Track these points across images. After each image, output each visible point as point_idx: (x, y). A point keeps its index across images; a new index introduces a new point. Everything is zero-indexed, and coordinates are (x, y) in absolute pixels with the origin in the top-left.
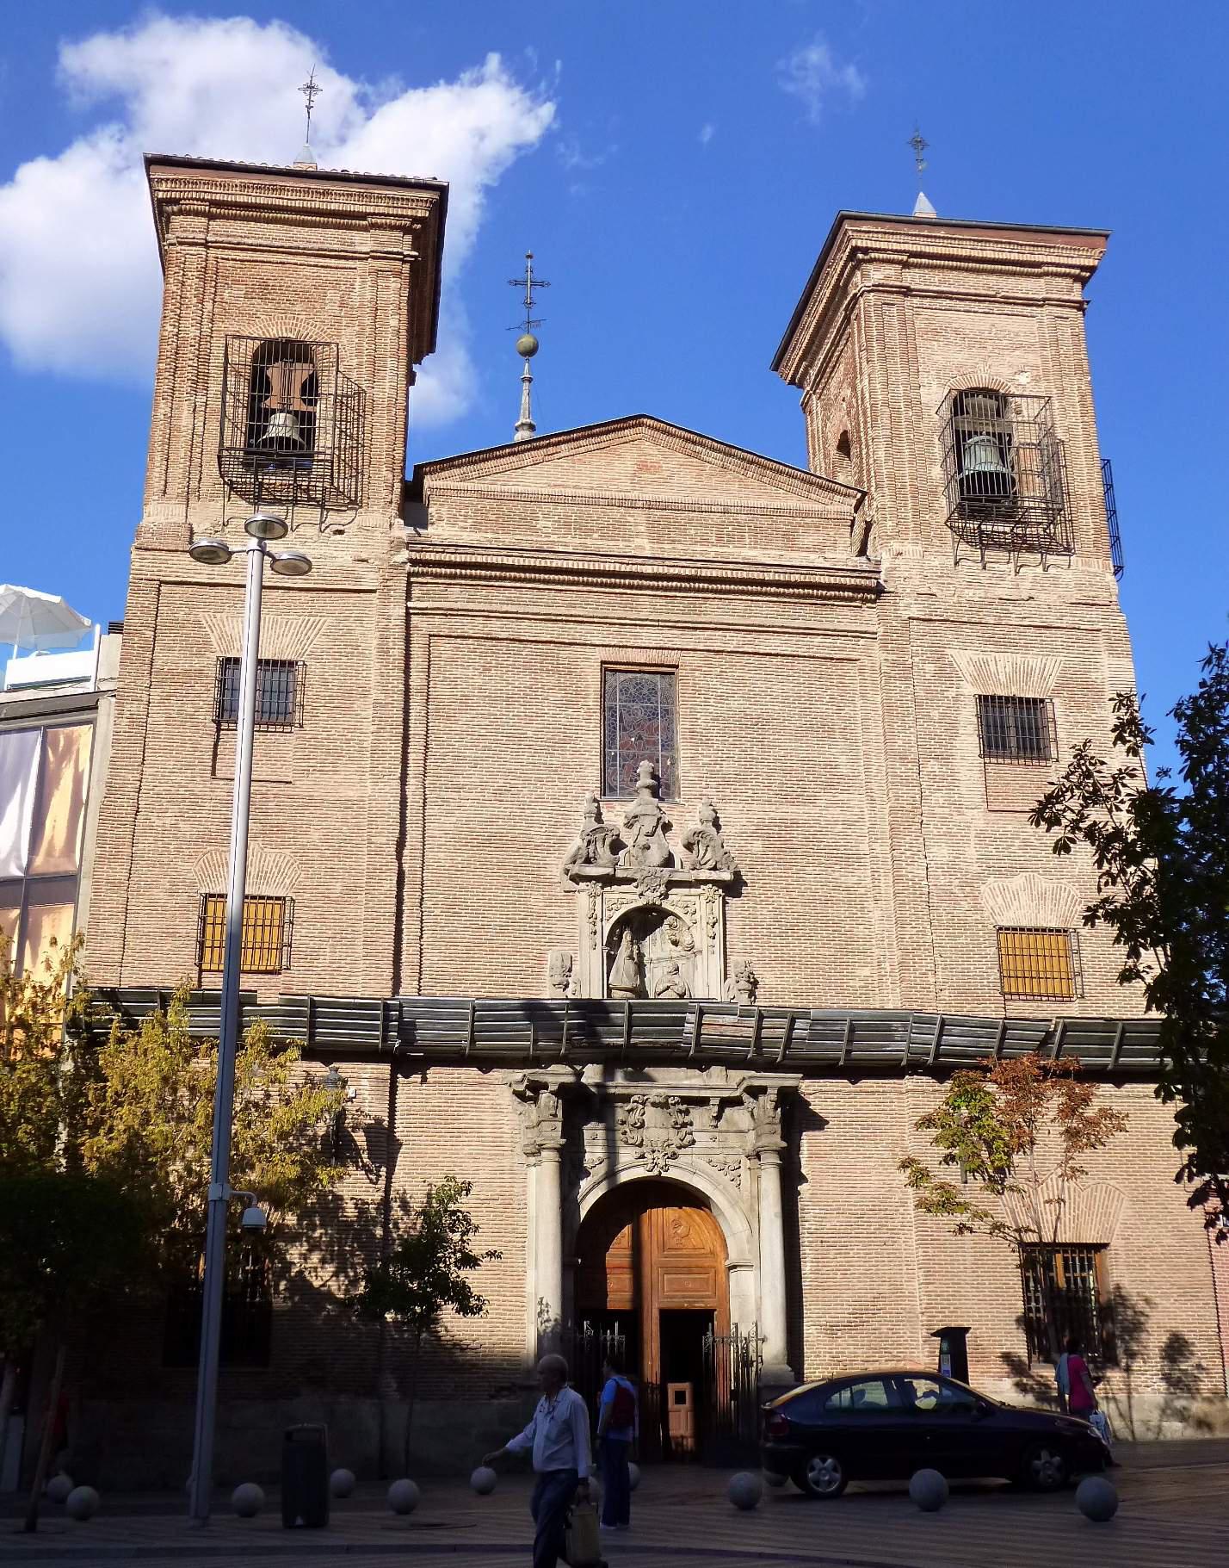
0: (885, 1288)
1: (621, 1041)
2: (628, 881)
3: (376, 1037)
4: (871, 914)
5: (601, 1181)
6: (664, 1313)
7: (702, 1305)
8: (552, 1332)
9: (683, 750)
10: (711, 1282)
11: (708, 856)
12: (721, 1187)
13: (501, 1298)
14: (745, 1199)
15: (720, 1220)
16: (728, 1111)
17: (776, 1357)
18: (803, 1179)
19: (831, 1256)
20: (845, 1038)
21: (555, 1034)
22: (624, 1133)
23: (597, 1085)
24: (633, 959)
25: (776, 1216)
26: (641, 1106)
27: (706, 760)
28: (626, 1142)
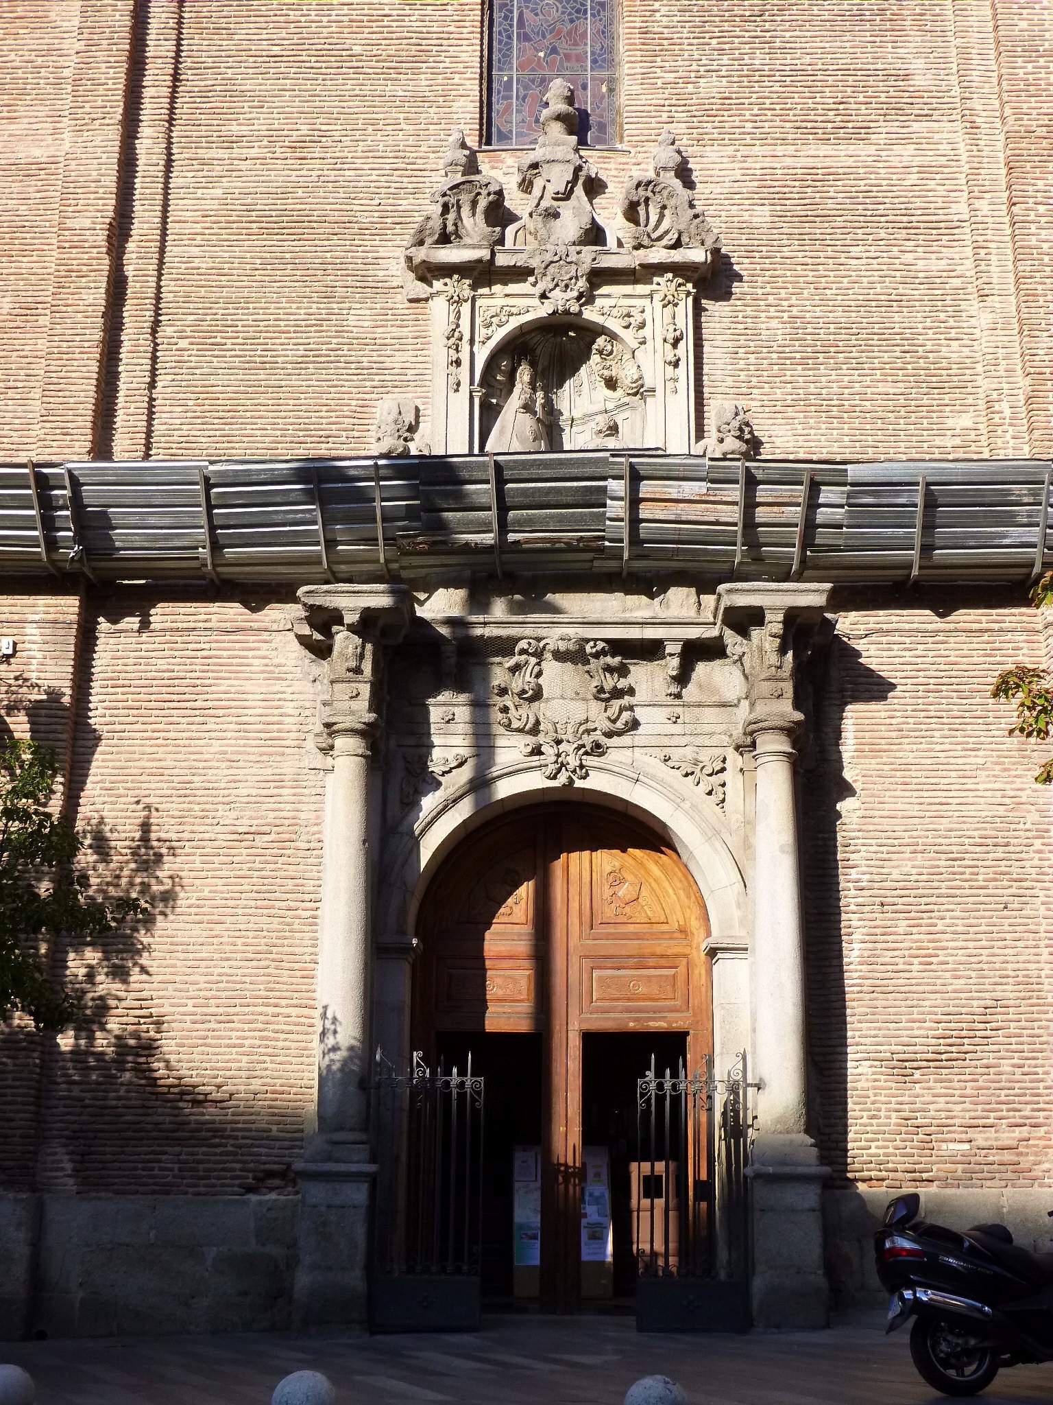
0: (1008, 991)
1: (488, 538)
2: (519, 274)
3: (33, 542)
4: (973, 321)
5: (460, 797)
6: (591, 1040)
7: (664, 1025)
8: (342, 1070)
9: (629, 65)
10: (680, 982)
11: (665, 225)
12: (686, 805)
13: (271, 1010)
14: (734, 827)
15: (692, 867)
16: (702, 670)
17: (779, 1120)
18: (846, 790)
19: (901, 930)
20: (918, 521)
21: (363, 529)
22: (505, 710)
23: (451, 622)
24: (535, 413)
25: (782, 851)
26: (533, 660)
27: (670, 77)
28: (508, 726)
